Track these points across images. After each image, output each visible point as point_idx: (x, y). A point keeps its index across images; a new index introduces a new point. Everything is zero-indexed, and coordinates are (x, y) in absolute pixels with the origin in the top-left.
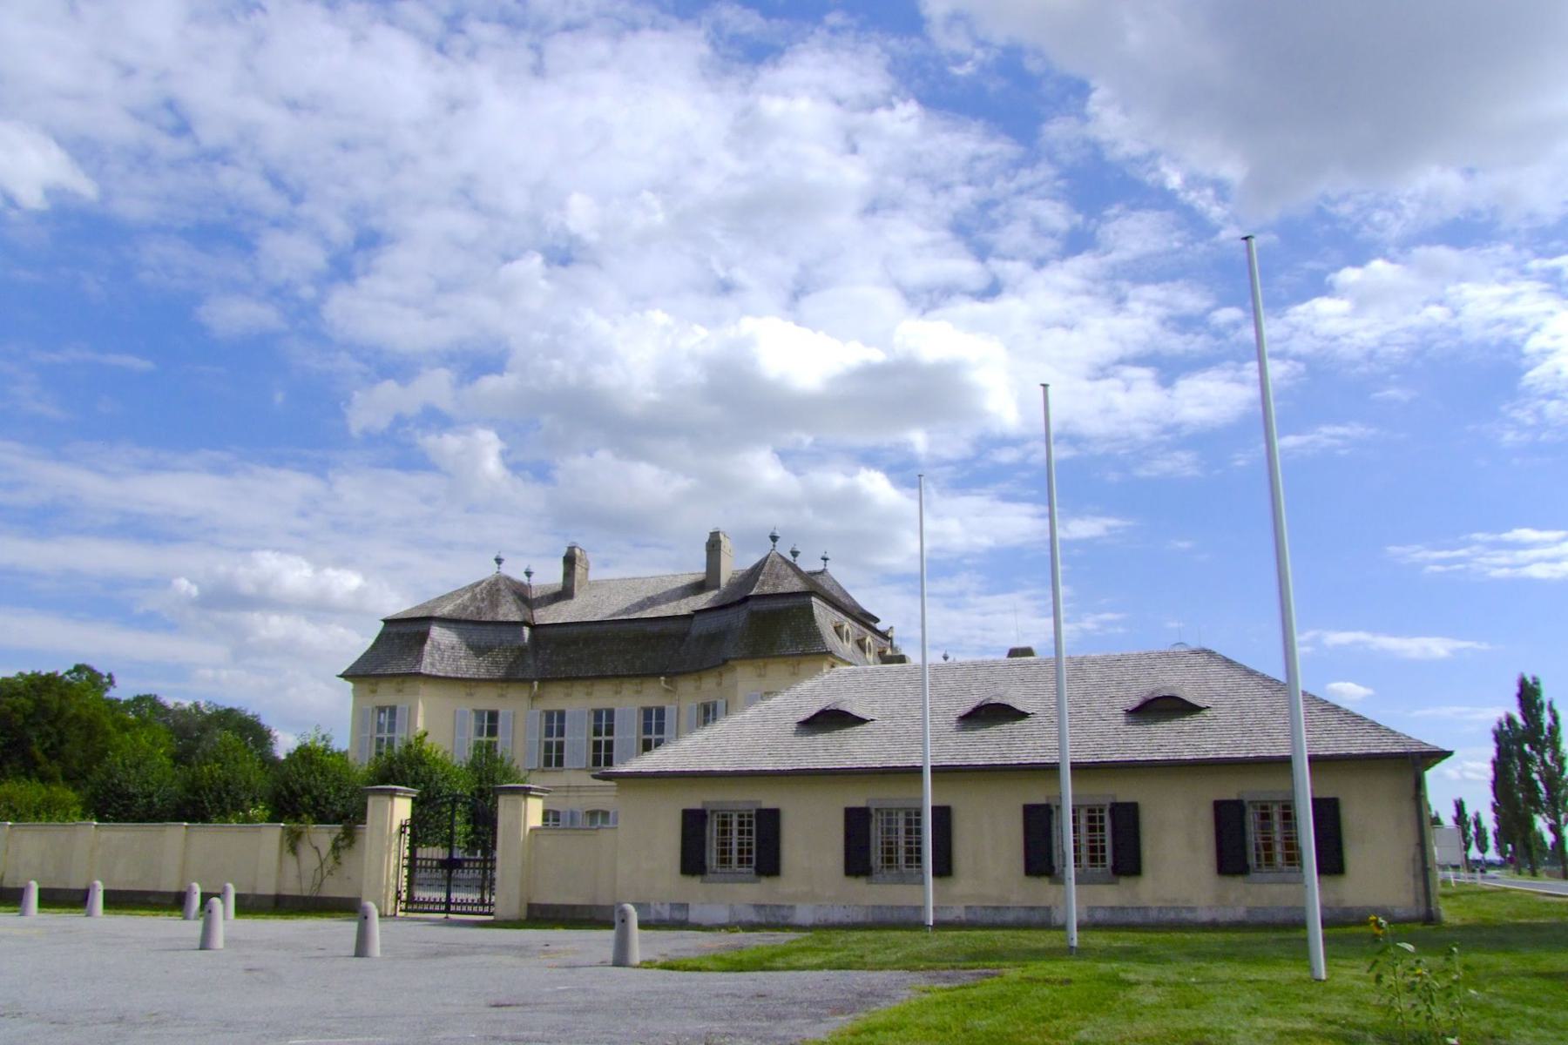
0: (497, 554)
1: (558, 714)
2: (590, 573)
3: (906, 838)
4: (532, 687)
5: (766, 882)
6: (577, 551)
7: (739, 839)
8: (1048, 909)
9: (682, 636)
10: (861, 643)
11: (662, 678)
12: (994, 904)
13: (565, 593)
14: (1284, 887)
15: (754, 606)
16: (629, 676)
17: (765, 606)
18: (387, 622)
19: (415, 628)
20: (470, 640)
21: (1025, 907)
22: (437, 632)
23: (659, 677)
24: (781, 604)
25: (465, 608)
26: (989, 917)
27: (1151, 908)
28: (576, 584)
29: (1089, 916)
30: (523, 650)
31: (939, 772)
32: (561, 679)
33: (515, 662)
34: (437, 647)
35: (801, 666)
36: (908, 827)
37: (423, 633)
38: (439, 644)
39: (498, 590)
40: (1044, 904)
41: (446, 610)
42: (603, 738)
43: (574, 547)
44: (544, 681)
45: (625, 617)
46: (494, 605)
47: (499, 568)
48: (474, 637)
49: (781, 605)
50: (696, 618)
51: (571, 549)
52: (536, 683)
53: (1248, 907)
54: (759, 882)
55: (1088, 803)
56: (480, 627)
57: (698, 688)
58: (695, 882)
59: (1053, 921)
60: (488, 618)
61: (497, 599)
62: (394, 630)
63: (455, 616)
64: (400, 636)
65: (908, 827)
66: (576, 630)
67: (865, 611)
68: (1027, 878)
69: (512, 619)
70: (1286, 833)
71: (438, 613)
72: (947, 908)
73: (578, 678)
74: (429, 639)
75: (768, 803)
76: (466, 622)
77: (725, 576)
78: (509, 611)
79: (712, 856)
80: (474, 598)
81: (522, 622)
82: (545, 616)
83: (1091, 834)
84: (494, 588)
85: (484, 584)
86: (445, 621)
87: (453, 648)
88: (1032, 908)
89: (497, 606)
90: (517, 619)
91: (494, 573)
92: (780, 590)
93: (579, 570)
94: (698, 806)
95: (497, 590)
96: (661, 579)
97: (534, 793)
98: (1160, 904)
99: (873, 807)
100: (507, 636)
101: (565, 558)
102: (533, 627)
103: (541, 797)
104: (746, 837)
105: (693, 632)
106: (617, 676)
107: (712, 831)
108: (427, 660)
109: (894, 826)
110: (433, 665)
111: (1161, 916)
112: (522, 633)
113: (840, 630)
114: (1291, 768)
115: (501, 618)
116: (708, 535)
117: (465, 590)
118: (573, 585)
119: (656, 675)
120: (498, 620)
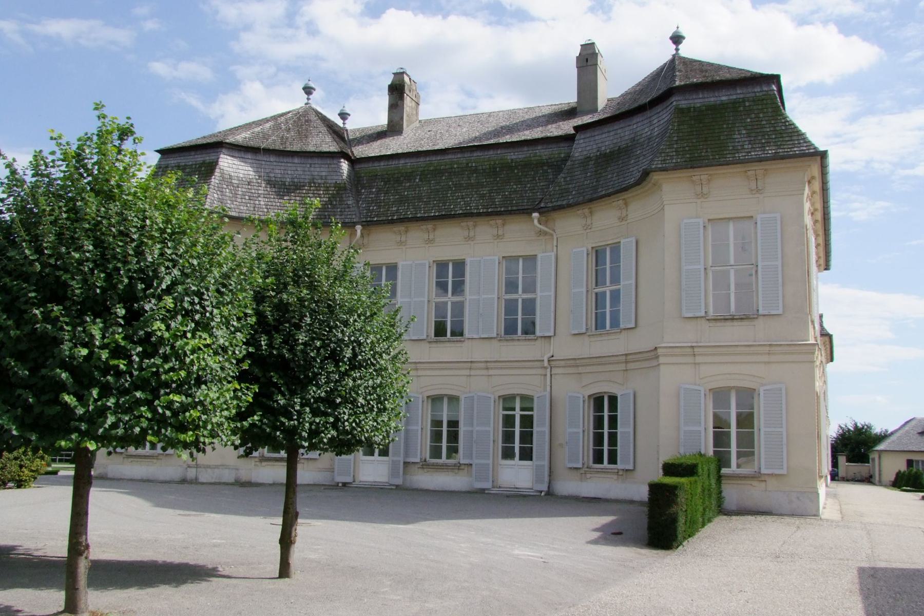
1: (387, 268)
4: (353, 234)
6: (406, 79)
7: (531, 409)
9: (557, 166)
11: (535, 215)
16: (488, 214)
17: (699, 100)
19: (200, 158)
20: (272, 175)
22: (227, 163)
23: (530, 214)
25: (265, 136)
30: (340, 189)
32: (392, 222)
33: (330, 202)
34: (227, 180)
37: (210, 163)
41: (239, 138)
42: (450, 298)
44: (368, 224)
47: (308, 99)
48: (277, 171)
51: (399, 75)
52: (359, 228)
55: (830, 395)
57: (587, 227)
60: (296, 148)
62: (172, 161)
66: (410, 163)
71: (230, 139)
73: (415, 219)
74: (217, 170)
76: (268, 151)
77: (601, 103)
80: (277, 127)
81: (338, 153)
85: (290, 115)
87: (249, 183)
91: (303, 105)
93: (408, 102)
95: (307, 121)
96: (514, 112)
97: (393, 487)
100: (319, 170)
101: (390, 86)
103: (360, 482)
106: (468, 215)
112: (339, 167)
115: (311, 148)
116: (580, 47)
117: (267, 120)
118: (402, 118)
119: (527, 212)
120: (308, 150)
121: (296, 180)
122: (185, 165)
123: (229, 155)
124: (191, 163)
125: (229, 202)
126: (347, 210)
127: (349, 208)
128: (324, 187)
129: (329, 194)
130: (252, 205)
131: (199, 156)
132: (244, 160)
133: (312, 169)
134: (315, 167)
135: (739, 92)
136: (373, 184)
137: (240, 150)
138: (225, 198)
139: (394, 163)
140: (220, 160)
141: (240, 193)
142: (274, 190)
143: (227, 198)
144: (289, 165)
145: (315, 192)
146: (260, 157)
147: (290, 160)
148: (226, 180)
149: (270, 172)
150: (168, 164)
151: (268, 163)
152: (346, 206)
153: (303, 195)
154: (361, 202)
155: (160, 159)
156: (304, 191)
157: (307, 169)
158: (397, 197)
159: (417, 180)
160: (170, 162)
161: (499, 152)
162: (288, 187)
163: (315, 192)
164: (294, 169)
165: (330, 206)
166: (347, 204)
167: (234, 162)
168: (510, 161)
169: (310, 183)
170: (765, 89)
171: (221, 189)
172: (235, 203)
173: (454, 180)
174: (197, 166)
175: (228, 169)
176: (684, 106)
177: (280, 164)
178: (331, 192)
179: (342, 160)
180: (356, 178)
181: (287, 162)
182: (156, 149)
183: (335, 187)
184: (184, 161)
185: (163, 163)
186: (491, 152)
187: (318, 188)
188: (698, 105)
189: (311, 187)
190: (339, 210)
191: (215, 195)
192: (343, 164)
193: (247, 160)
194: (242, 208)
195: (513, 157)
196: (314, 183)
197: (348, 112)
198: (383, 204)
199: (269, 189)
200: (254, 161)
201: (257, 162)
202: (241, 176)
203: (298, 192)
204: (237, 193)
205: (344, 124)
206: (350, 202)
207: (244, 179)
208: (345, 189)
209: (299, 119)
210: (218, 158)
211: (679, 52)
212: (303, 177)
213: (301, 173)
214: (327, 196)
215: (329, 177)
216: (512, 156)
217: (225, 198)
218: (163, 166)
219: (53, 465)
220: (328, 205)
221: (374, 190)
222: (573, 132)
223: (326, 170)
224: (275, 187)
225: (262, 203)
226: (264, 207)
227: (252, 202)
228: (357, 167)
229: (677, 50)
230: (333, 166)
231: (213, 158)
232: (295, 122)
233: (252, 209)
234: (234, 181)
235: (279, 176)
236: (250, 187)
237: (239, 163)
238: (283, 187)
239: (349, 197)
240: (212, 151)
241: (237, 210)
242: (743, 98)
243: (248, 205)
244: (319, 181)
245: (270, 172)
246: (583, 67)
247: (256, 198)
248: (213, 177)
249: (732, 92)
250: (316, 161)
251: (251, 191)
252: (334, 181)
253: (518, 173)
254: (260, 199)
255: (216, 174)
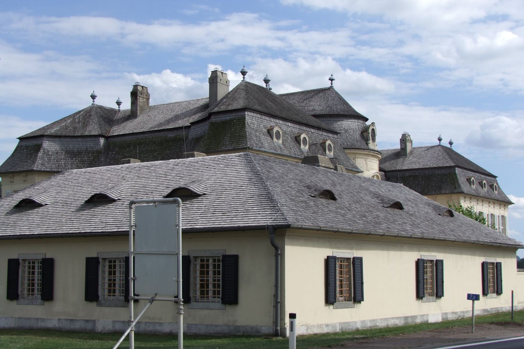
0: (242, 68)
2: (150, 100)
3: (201, 277)
5: (229, 309)
6: (140, 88)
8: (94, 321)
10: (298, 138)
12: (71, 318)
13: (132, 115)
14: (207, 311)
15: (213, 119)
18: (21, 139)
20: (68, 148)
21: (85, 320)
22: (47, 144)
24: (228, 117)
25: (66, 127)
26: (67, 326)
27: (142, 322)
28: (138, 108)
29: (113, 327)
30: (99, 152)
31: (184, 233)
34: (46, 153)
35: (15, 178)
36: (208, 270)
37: (38, 145)
38: (48, 151)
39: (90, 115)
40: (93, 319)
43: (137, 85)
45: (156, 129)
46: (85, 125)
47: (94, 101)
48: (71, 146)
49: (228, 118)
50: (192, 128)
53: (188, 324)
54: (44, 305)
56: (74, 140)
58: (14, 303)
59: (96, 329)
61: (88, 122)
62: (24, 143)
63: (59, 133)
64: (27, 147)
65: (208, 270)
67: (356, 112)
68: (325, 306)
69: (93, 133)
70: (109, 277)
71: (48, 133)
72: (50, 319)
74: (42, 149)
75: (231, 251)
76: (65, 137)
78: (93, 129)
79: (103, 290)
80: (73, 122)
82: (117, 130)
83: (34, 278)
84: (88, 114)
86: (53, 137)
87: (57, 153)
88: (87, 321)
89: (87, 126)
90: (96, 133)
91: (91, 105)
92: (230, 108)
94: (95, 255)
98: (147, 320)
99: (101, 257)
102: (107, 138)
104: (112, 276)
105: (190, 137)
107: (104, 272)
108: (39, 161)
109: (31, 270)
110: (43, 164)
111: (146, 328)
112: (99, 142)
113: (271, 132)
114: (129, 237)
118: (137, 109)
121: (79, 150)
122: (29, 146)
123: (47, 141)
124: (31, 145)
125: (47, 164)
126: (101, 163)
127: (101, 162)
128: (92, 152)
129: (93, 156)
130: (58, 164)
131: (35, 141)
132: (55, 142)
133: (87, 144)
134: (88, 143)
135: (233, 115)
136: (114, 149)
137: (53, 137)
138: (45, 162)
139: (124, 138)
140: (43, 143)
141: (52, 158)
142: (69, 155)
143: (46, 162)
144: (76, 142)
145: (88, 155)
146: (62, 139)
147: (76, 140)
148: (46, 153)
149: (67, 147)
150: (22, 145)
151: (66, 142)
152: (101, 162)
153: (82, 157)
154: (107, 159)
155: (19, 142)
156: (83, 155)
157: (84, 144)
158: (122, 156)
159: (132, 148)
160: (23, 144)
161: (165, 133)
162: (75, 154)
163: (88, 155)
164: (78, 144)
165: (93, 162)
166: (101, 161)
167: (50, 144)
168: (169, 137)
169: (85, 151)
170: (242, 114)
171: (43, 158)
172: (49, 164)
173: (146, 147)
174: (34, 146)
175: (47, 147)
176: (214, 122)
177: (72, 142)
178: (95, 155)
179: (101, 138)
180: (107, 146)
181: (75, 141)
182: (18, 137)
183: (97, 152)
184: (29, 143)
185: (20, 144)
186: (162, 133)
187: (89, 153)
188: (218, 121)
189: (86, 152)
190: (97, 164)
191: (40, 162)
192: (101, 140)
193: (56, 142)
194: (53, 166)
195: (170, 136)
196: (87, 150)
197: (121, 102)
198: (116, 160)
199: (66, 155)
200: (59, 142)
201: (61, 142)
202: (53, 150)
203: (80, 155)
204: (51, 159)
205: (451, 147)
206: (102, 160)
207: (55, 151)
208: (101, 153)
209: (86, 114)
210: (42, 143)
211: (245, 79)
212: (82, 148)
213: (82, 146)
214: (93, 157)
215: (94, 147)
216: (171, 135)
217: (45, 162)
218: (20, 146)
219: (346, 336)
220: (92, 161)
221: (114, 152)
222: (189, 125)
223: (93, 143)
224: (69, 154)
225: (63, 163)
226: (63, 164)
227: (58, 163)
228: (110, 140)
229: (440, 143)
230: (96, 141)
231: (40, 142)
232: (83, 116)
233: (57, 166)
234: (50, 153)
235: (71, 148)
236: (57, 155)
237: (52, 144)
238: (73, 153)
239: (102, 157)
240: (40, 139)
241: (50, 168)
242: (234, 118)
243: (56, 164)
244: (90, 149)
245: (67, 147)
246: (212, 83)
247: (60, 161)
248: (40, 152)
249: (231, 115)
250: (88, 139)
251: (58, 157)
252: (96, 149)
253: (171, 144)
254: (62, 161)
255: (41, 151)
